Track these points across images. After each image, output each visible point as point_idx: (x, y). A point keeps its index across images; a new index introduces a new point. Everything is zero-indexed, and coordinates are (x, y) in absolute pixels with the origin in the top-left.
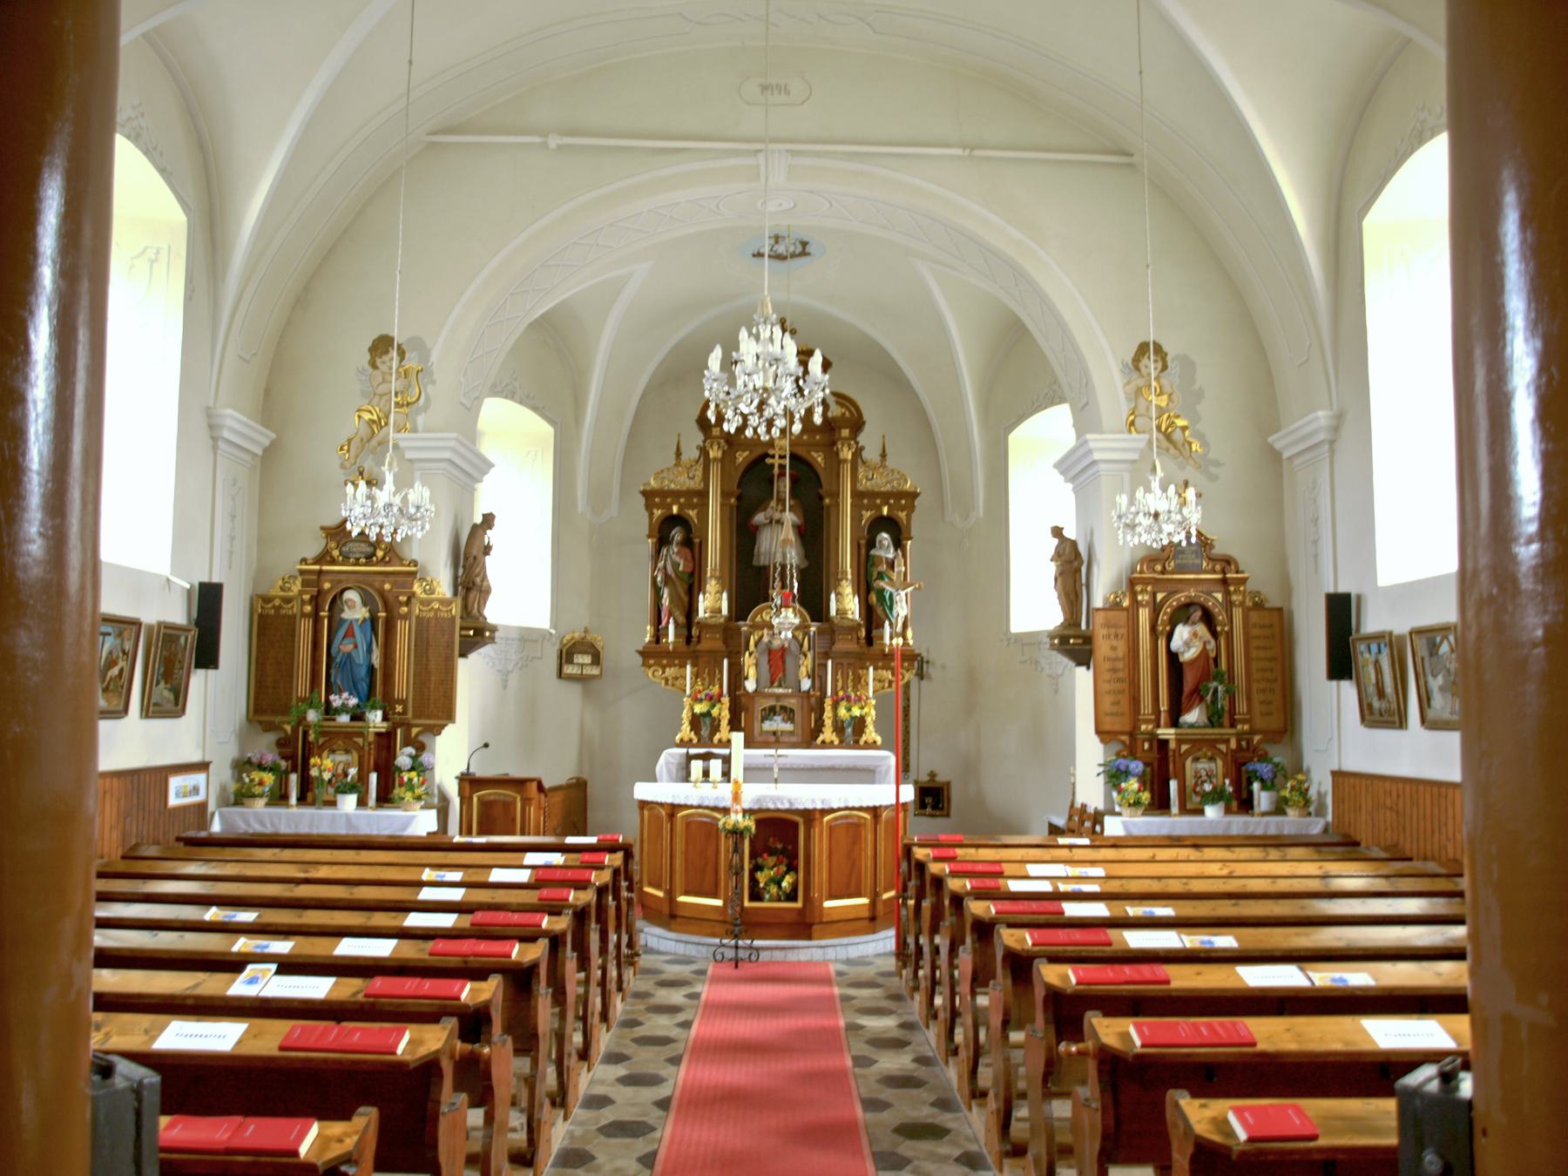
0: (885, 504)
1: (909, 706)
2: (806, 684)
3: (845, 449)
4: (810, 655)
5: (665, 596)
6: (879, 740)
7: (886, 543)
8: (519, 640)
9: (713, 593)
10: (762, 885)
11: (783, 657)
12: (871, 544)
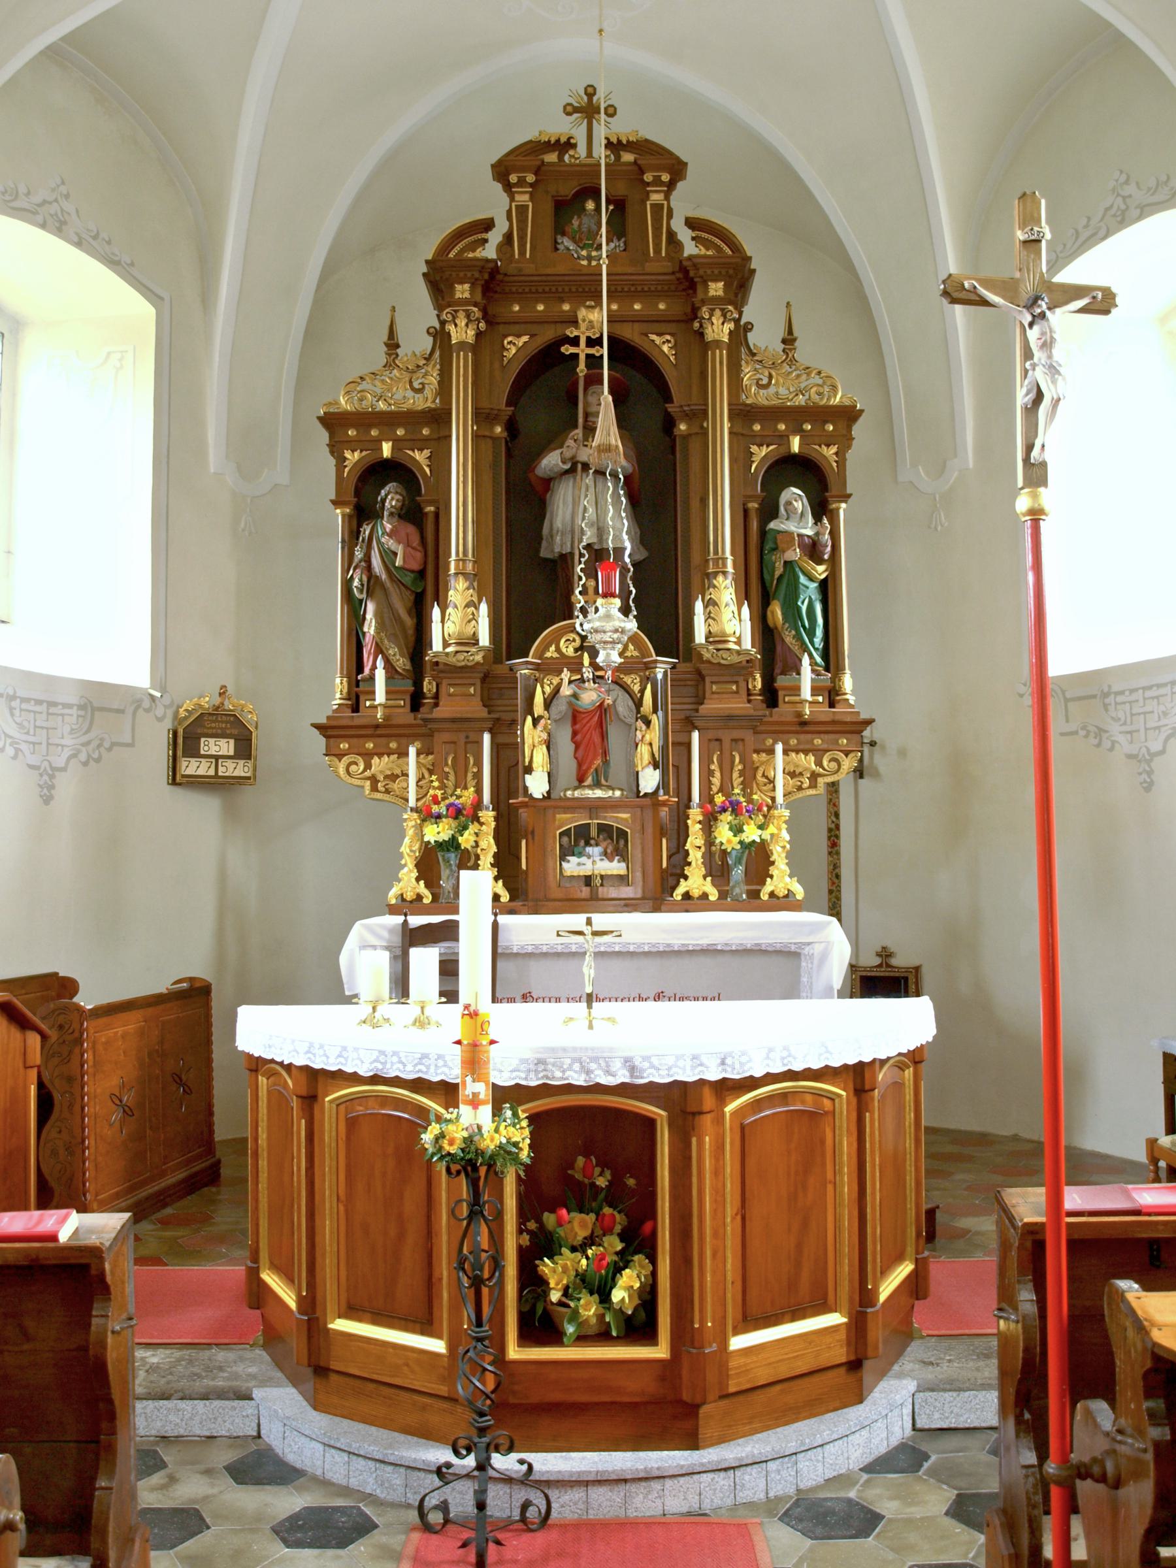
0: (795, 433)
1: (838, 827)
2: (650, 780)
3: (717, 319)
4: (655, 721)
5: (369, 616)
6: (799, 892)
7: (798, 505)
8: (81, 707)
9: (460, 606)
10: (555, 1296)
11: (601, 726)
12: (770, 510)
